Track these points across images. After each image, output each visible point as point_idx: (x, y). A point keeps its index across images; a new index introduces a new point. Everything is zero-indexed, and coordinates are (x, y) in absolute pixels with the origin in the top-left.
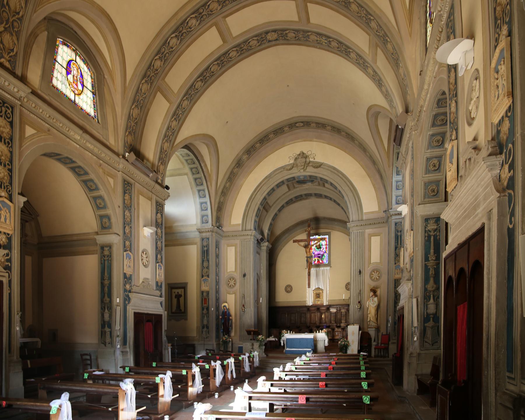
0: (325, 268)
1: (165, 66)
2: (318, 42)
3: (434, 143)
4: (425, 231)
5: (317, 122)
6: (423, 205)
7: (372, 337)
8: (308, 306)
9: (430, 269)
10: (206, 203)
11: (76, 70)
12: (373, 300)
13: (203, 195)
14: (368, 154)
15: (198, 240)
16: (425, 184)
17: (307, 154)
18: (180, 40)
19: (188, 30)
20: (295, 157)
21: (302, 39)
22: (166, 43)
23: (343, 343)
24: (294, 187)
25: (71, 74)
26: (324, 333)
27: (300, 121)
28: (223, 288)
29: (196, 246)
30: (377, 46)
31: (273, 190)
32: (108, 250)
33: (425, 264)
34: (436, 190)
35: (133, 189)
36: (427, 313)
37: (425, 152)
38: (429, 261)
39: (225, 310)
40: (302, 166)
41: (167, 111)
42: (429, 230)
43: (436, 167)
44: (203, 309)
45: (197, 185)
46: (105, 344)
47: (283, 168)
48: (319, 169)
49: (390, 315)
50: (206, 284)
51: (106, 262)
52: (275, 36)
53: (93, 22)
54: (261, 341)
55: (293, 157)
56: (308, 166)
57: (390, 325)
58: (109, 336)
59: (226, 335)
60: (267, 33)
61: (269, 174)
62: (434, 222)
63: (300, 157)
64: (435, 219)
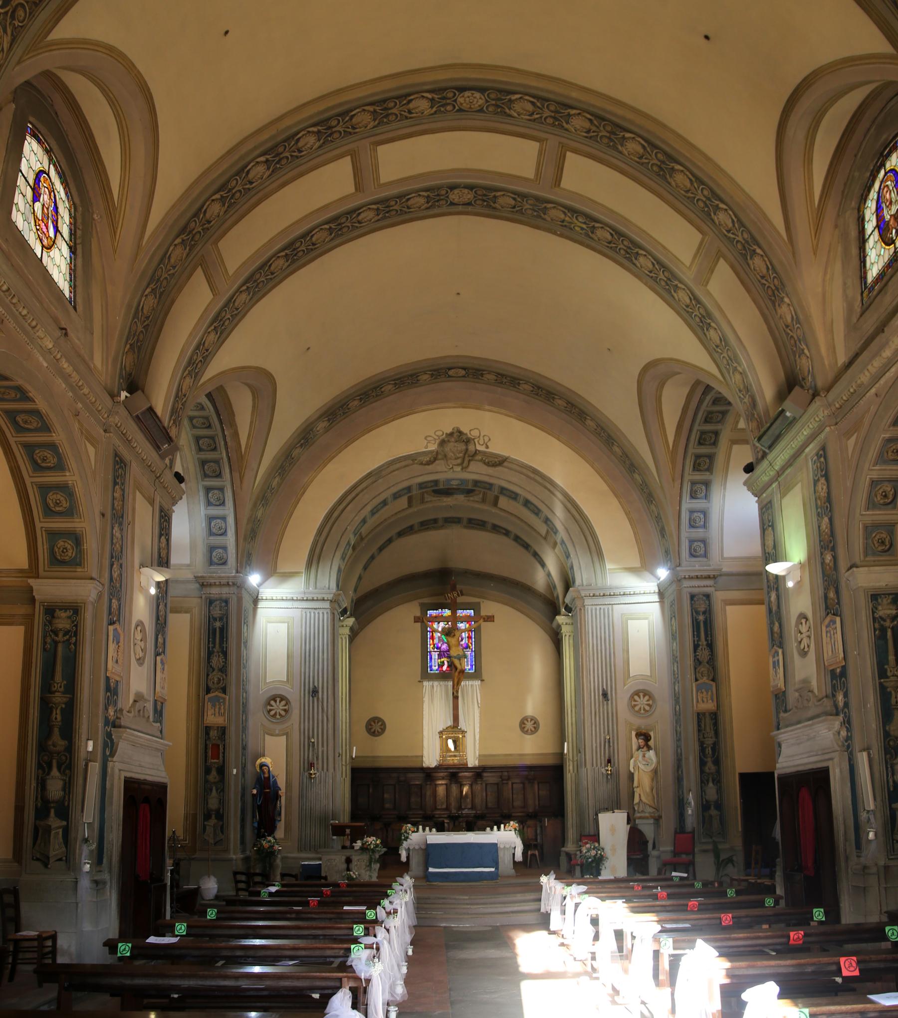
0: (471, 683)
1: (227, 216)
2: (565, 224)
3: (890, 453)
4: (874, 619)
5: (501, 372)
6: (866, 569)
7: (648, 839)
8: (429, 768)
9: (890, 693)
10: (224, 518)
11: (48, 193)
12: (644, 756)
13: (218, 499)
14: (616, 449)
15: (195, 603)
16: (866, 527)
17: (469, 436)
18: (271, 170)
19: (293, 154)
20: (441, 438)
21: (530, 212)
22: (242, 171)
23: (593, 853)
24: (422, 501)
25: (39, 201)
26: (513, 832)
27: (460, 365)
28: (256, 719)
29: (188, 616)
30: (719, 255)
31: (384, 503)
32: (69, 617)
33: (881, 684)
34: (887, 540)
35: (127, 475)
36: (894, 782)
37: (869, 469)
38: (887, 677)
39: (264, 773)
40: (458, 458)
41: (206, 309)
42: (881, 617)
43: (888, 499)
44: (208, 771)
45: (206, 476)
46: (45, 861)
47: (412, 459)
48: (499, 468)
49: (690, 790)
50: (217, 710)
51: (60, 648)
52: (468, 196)
53: (113, 102)
54: (373, 851)
55: (437, 438)
56: (472, 460)
57: (692, 811)
58: (61, 840)
59: (269, 836)
60: (452, 187)
61: (375, 470)
62: (889, 601)
63: (453, 440)
64: (891, 597)
